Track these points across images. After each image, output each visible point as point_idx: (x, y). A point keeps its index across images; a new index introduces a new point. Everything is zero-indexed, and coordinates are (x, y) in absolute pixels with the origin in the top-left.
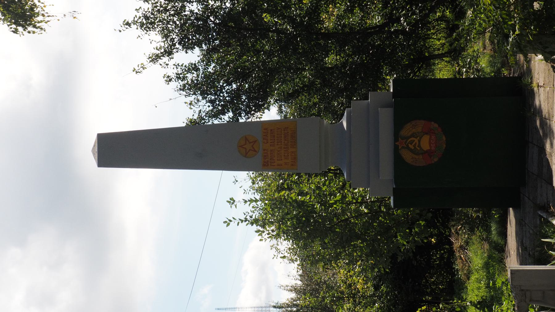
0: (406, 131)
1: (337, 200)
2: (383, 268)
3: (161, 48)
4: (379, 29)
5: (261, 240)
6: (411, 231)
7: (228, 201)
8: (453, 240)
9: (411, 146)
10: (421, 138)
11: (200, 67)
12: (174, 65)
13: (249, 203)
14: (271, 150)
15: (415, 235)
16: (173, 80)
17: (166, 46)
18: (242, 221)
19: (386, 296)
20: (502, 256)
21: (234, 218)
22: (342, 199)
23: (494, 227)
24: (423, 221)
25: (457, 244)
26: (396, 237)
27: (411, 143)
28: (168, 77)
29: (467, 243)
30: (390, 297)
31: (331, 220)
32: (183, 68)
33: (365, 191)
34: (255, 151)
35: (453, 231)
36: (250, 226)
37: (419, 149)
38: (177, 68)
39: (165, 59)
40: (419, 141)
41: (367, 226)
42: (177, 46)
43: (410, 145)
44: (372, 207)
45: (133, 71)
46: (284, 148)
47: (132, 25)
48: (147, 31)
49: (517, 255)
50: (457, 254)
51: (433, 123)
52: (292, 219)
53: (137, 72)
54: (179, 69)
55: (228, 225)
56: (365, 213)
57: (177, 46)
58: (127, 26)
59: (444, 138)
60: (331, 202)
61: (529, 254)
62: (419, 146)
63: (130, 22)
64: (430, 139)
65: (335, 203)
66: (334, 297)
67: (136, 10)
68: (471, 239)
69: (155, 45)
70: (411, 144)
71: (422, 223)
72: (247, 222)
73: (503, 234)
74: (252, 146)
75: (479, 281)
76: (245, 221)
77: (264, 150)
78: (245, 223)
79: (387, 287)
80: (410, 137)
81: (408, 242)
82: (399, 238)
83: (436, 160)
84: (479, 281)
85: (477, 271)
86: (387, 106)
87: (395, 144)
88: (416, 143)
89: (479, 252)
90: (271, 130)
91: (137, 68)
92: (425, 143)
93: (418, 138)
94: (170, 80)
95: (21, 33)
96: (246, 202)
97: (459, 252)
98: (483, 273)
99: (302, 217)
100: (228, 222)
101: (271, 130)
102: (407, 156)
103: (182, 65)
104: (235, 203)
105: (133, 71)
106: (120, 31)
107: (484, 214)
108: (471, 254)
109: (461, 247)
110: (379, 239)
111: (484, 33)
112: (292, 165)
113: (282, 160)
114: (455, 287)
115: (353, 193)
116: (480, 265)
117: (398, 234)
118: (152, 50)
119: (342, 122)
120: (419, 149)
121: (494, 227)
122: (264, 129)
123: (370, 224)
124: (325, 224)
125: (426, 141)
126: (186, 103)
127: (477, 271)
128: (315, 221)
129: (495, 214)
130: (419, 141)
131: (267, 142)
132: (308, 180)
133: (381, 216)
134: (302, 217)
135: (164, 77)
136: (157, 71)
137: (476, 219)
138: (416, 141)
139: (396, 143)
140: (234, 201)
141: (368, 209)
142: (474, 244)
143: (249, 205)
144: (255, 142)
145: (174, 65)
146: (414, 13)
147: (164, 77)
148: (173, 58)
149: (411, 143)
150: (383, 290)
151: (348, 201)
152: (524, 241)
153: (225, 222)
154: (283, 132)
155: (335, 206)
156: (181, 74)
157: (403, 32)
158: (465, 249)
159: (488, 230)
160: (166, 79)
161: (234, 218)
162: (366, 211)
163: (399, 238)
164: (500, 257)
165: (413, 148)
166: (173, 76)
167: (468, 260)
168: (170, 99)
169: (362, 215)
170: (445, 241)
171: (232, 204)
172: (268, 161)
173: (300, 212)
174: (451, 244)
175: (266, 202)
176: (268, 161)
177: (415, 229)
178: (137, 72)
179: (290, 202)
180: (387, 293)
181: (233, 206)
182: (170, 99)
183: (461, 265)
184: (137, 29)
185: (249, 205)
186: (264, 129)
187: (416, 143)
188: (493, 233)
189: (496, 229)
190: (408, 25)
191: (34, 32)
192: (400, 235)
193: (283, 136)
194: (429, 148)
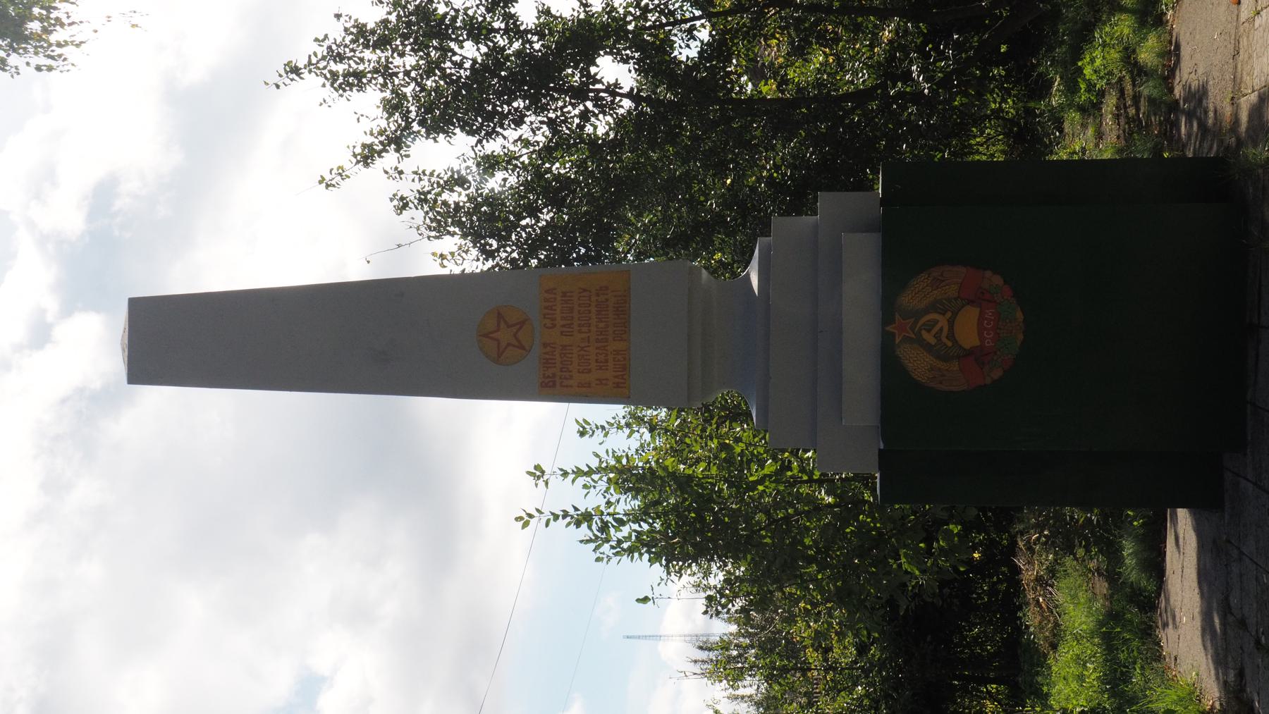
0: (908, 299)
1: (765, 476)
2: (866, 629)
3: (381, 133)
4: (861, 97)
5: (598, 560)
6: (930, 546)
7: (529, 473)
8: (1020, 563)
9: (929, 338)
10: (955, 314)
11: (470, 178)
12: (415, 173)
13: (571, 477)
14: (564, 347)
15: (940, 555)
16: (411, 205)
17: (393, 128)
18: (556, 517)
19: (880, 672)
20: (1150, 619)
21: (538, 510)
22: (777, 473)
23: (1128, 549)
24: (956, 524)
25: (1030, 572)
26: (897, 558)
27: (929, 327)
28: (402, 198)
29: (1052, 572)
30: (888, 673)
31: (748, 519)
32: (433, 179)
33: (827, 458)
34: (522, 348)
35: (1021, 544)
36: (572, 527)
37: (950, 344)
38: (420, 179)
39: (390, 158)
40: (951, 323)
41: (831, 535)
42: (415, 127)
43: (925, 335)
44: (844, 492)
45: (320, 182)
46: (597, 341)
47: (306, 74)
48: (344, 90)
49: (1203, 630)
50: (1031, 595)
51: (988, 273)
52: (666, 514)
53: (328, 186)
54: (425, 182)
55: (526, 525)
56: (829, 505)
57: (415, 127)
58: (294, 76)
59: (1019, 315)
60: (751, 479)
61: (1258, 642)
62: (951, 336)
63: (300, 65)
64: (981, 317)
65: (761, 481)
66: (774, 668)
67: (316, 40)
68: (1062, 565)
69: (366, 125)
70: (929, 331)
71: (956, 529)
72: (568, 519)
73: (1155, 566)
74: (515, 335)
75: (1080, 661)
76: (564, 517)
77: (545, 345)
78: (562, 522)
79: (883, 650)
80: (927, 311)
81: (923, 572)
82: (903, 560)
83: (997, 374)
84: (1080, 661)
85: (1077, 638)
86: (868, 229)
87: (883, 329)
88: (941, 329)
89: (1082, 597)
90: (564, 294)
91: (328, 177)
92: (968, 329)
93: (949, 315)
94: (405, 206)
95: (13, 70)
96: (565, 474)
97: (1035, 589)
98: (1092, 648)
99: (689, 509)
100: (526, 518)
101: (564, 294)
102: (918, 364)
103: (432, 174)
104: (545, 477)
105: (320, 182)
106: (278, 87)
107: (1104, 516)
108: (1061, 597)
109: (1039, 579)
110: (858, 566)
111: (1097, 106)
112: (618, 385)
113: (590, 371)
114: (1020, 667)
115: (802, 460)
116: (1085, 627)
117: (902, 552)
118: (360, 136)
119: (748, 275)
120: (950, 344)
121: (1128, 549)
122: (547, 291)
123: (838, 530)
124: (737, 529)
125: (967, 325)
126: (434, 254)
127: (1077, 638)
128: (717, 521)
129: (1135, 519)
130: (951, 323)
131: (554, 326)
132: (704, 430)
133: (863, 513)
134: (689, 509)
135: (391, 200)
136: (375, 184)
137: (1083, 527)
138: (943, 322)
139: (889, 328)
140: (543, 472)
141: (835, 496)
142: (1067, 575)
143: (573, 481)
144: (522, 324)
145: (415, 173)
146: (941, 55)
147: (391, 200)
148: (408, 156)
149: (929, 327)
150: (873, 655)
151: (791, 477)
152: (1234, 601)
153: (518, 519)
154: (594, 298)
155: (761, 488)
156: (429, 192)
157: (917, 97)
158: (1047, 584)
159: (1113, 554)
160: (395, 202)
161: (538, 510)
162: (831, 500)
163: (903, 560)
164: (1145, 623)
165: (933, 341)
166: (412, 196)
167: (1052, 611)
168: (399, 246)
169: (820, 509)
170: (1002, 559)
171: (539, 478)
172: (554, 375)
173: (685, 500)
174: (1016, 571)
175: (612, 475)
176: (554, 375)
177: (938, 542)
178: (328, 186)
179: (661, 478)
180: (882, 664)
181: (541, 482)
182: (399, 246)
183: (1039, 618)
184: (324, 85)
185: (573, 481)
186: (547, 291)
187: (941, 329)
188: (1128, 562)
189: (1135, 554)
190: (925, 80)
191: (50, 69)
192: (906, 555)
193: (593, 309)
194: (977, 343)
